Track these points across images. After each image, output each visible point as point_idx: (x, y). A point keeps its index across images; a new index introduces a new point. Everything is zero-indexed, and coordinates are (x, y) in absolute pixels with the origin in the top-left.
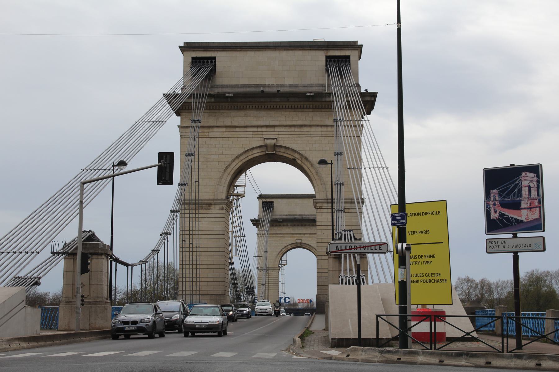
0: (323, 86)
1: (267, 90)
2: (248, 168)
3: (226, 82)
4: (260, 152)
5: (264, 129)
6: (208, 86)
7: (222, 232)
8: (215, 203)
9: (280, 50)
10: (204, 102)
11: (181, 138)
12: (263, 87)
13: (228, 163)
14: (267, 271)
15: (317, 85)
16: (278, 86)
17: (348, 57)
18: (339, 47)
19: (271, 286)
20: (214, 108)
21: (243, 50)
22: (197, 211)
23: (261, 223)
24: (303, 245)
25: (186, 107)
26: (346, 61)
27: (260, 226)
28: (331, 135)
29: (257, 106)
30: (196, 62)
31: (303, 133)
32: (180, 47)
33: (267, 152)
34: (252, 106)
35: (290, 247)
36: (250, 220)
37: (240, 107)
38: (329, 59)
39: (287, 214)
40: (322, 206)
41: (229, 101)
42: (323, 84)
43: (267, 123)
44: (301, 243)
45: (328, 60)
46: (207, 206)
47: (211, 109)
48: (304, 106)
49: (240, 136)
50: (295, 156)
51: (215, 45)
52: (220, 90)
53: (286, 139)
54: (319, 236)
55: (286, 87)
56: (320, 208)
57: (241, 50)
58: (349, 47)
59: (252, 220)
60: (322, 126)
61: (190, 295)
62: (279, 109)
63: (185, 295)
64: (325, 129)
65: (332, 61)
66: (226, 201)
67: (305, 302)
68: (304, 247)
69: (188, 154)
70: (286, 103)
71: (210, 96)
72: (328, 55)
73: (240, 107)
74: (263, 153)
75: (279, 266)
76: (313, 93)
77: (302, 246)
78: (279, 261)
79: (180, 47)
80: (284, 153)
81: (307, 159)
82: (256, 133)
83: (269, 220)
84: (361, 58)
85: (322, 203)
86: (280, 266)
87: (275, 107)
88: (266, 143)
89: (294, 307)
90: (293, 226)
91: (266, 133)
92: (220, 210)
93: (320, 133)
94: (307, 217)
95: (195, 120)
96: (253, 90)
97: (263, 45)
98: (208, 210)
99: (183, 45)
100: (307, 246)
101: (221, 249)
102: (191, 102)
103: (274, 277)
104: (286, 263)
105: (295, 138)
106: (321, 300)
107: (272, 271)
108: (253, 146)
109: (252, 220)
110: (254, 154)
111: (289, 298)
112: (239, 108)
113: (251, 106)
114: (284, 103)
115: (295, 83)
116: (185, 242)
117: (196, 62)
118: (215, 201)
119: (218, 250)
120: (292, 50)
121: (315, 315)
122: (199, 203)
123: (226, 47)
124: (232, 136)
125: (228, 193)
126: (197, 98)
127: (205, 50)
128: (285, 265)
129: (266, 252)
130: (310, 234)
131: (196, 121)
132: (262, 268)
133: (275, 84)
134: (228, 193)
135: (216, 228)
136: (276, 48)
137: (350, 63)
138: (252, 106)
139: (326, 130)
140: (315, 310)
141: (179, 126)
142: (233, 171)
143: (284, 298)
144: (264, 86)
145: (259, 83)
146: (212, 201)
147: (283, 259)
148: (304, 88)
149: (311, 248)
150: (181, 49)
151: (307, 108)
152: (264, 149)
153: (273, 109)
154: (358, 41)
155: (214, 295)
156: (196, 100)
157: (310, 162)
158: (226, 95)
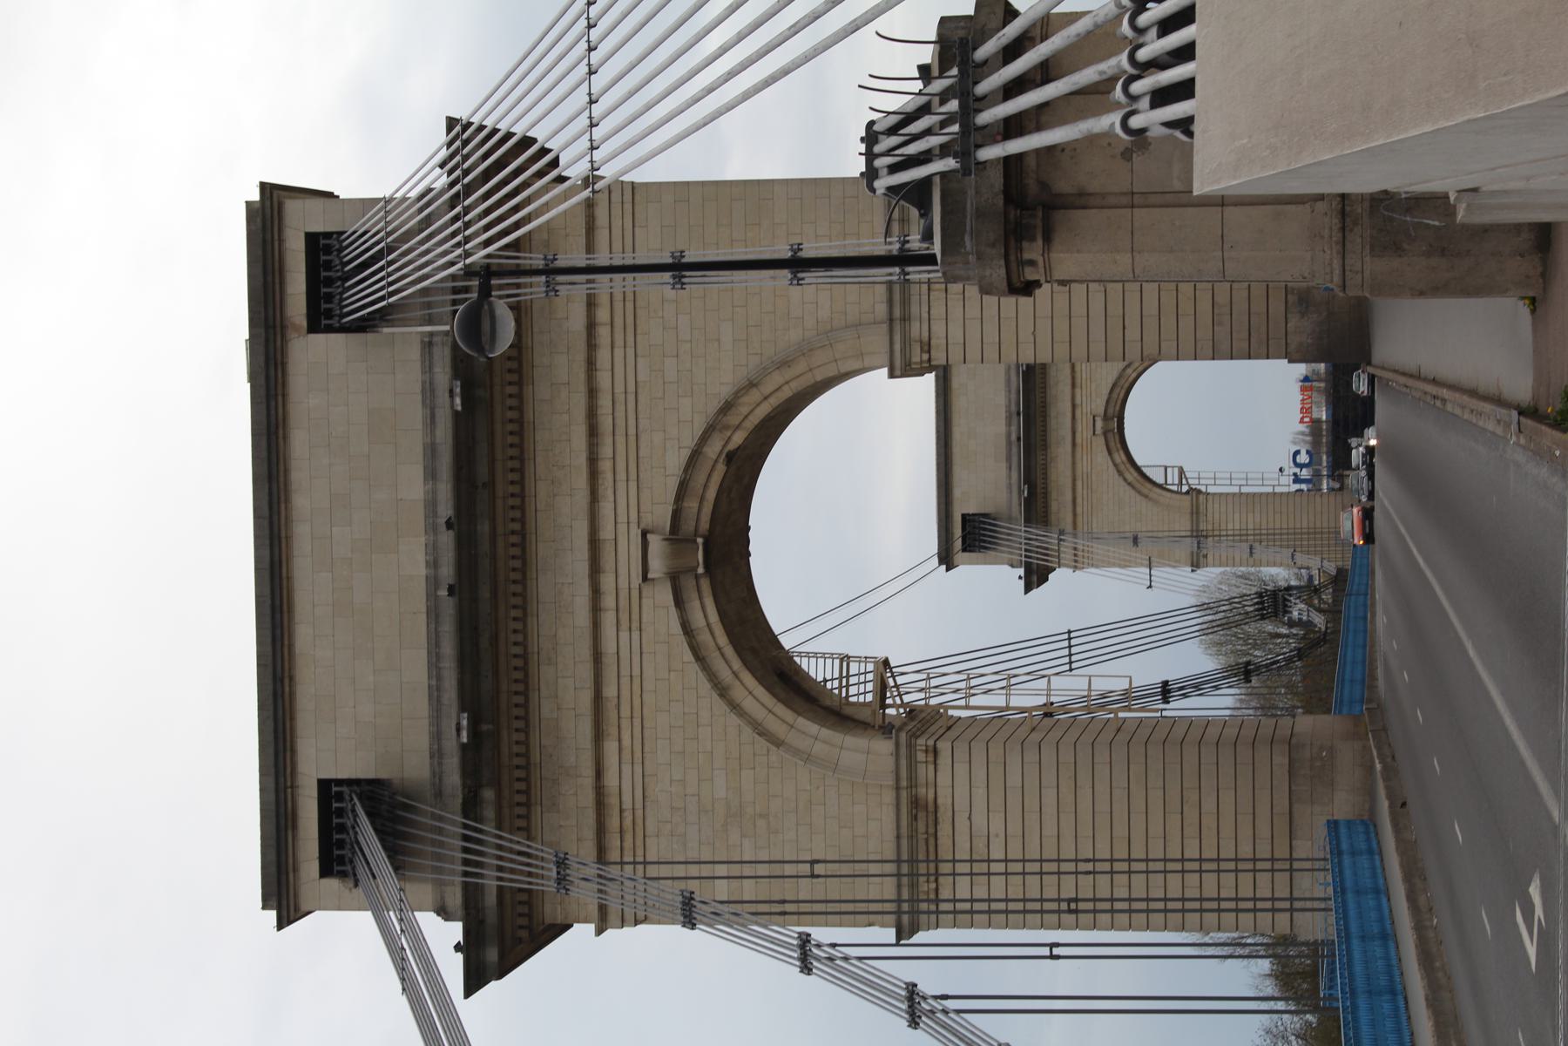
0: (428, 344)
1: (447, 572)
2: (774, 640)
3: (419, 740)
4: (701, 598)
5: (607, 582)
6: (434, 816)
7: (1031, 756)
8: (913, 783)
9: (286, 518)
11: (645, 920)
12: (436, 590)
13: (748, 731)
14: (1204, 533)
15: (428, 366)
16: (432, 528)
17: (312, 239)
18: (270, 279)
19: (1258, 520)
20: (522, 786)
21: (290, 669)
23: (1038, 559)
24: (1111, 411)
25: (520, 903)
26: (328, 250)
27: (1047, 561)
28: (630, 305)
29: (514, 613)
31: (621, 423)
32: (280, 926)
33: (701, 570)
34: (515, 631)
35: (1120, 457)
36: (1026, 593)
37: (516, 681)
38: (321, 318)
39: (1004, 465)
40: (921, 342)
41: (490, 727)
42: (422, 342)
44: (1106, 418)
45: (324, 322)
46: (921, 815)
47: (529, 799)
48: (511, 421)
49: (637, 681)
50: (715, 458)
51: (272, 786)
52: (453, 764)
53: (645, 494)
54: (1079, 351)
55: (434, 492)
56: (926, 348)
57: (291, 678)
58: (269, 236)
59: (1028, 588)
60: (591, 346)
61: (1292, 910)
62: (523, 521)
63: (1292, 899)
64: (603, 333)
65: (328, 306)
66: (903, 736)
67: (1309, 401)
68: (1117, 408)
69: (685, 917)
70: (500, 493)
71: (471, 807)
72: (305, 324)
73: (516, 681)
74: (705, 585)
75: (1187, 493)
76: (454, 382)
77: (1116, 414)
78: (1169, 494)
79: (280, 926)
81: (727, 407)
83: (1025, 531)
84: (333, 193)
85: (906, 342)
86: (1185, 488)
87: (514, 539)
88: (662, 575)
89: (1324, 433)
91: (623, 571)
92: (938, 762)
93: (619, 353)
94: (1013, 396)
95: (554, 874)
96: (448, 628)
97: (267, 591)
98: (941, 810)
99: (272, 915)
100: (1115, 395)
101: (1102, 756)
102: (500, 888)
103: (1223, 509)
104: (1176, 470)
105: (641, 454)
106: (1309, 341)
107: (1202, 518)
108: (676, 628)
109: (1028, 589)
110: (708, 625)
111: (1297, 453)
112: (520, 687)
113: (513, 638)
114: (499, 503)
115: (421, 458)
116: (1064, 912)
117: (341, 860)
118: (904, 783)
119: (1102, 771)
120: (286, 471)
121: (1376, 367)
122: (913, 861)
123: (276, 738)
124: (637, 714)
125: (874, 727)
127: (290, 824)
128: (1181, 472)
129: (1135, 540)
130: (1073, 386)
131: (558, 873)
132: (1192, 553)
133: (423, 539)
135: (1014, 779)
136: (280, 538)
138: (515, 631)
139: (609, 327)
140: (1335, 367)
141: (599, 932)
142: (780, 709)
143: (1297, 470)
144: (433, 582)
146: (904, 794)
147: (1160, 480)
148: (437, 420)
149: (1122, 381)
150: (290, 922)
151: (520, 409)
152: (688, 583)
153: (523, 545)
154: (246, 202)
155: (1293, 788)
156: (492, 870)
157: (739, 393)
158: (465, 740)
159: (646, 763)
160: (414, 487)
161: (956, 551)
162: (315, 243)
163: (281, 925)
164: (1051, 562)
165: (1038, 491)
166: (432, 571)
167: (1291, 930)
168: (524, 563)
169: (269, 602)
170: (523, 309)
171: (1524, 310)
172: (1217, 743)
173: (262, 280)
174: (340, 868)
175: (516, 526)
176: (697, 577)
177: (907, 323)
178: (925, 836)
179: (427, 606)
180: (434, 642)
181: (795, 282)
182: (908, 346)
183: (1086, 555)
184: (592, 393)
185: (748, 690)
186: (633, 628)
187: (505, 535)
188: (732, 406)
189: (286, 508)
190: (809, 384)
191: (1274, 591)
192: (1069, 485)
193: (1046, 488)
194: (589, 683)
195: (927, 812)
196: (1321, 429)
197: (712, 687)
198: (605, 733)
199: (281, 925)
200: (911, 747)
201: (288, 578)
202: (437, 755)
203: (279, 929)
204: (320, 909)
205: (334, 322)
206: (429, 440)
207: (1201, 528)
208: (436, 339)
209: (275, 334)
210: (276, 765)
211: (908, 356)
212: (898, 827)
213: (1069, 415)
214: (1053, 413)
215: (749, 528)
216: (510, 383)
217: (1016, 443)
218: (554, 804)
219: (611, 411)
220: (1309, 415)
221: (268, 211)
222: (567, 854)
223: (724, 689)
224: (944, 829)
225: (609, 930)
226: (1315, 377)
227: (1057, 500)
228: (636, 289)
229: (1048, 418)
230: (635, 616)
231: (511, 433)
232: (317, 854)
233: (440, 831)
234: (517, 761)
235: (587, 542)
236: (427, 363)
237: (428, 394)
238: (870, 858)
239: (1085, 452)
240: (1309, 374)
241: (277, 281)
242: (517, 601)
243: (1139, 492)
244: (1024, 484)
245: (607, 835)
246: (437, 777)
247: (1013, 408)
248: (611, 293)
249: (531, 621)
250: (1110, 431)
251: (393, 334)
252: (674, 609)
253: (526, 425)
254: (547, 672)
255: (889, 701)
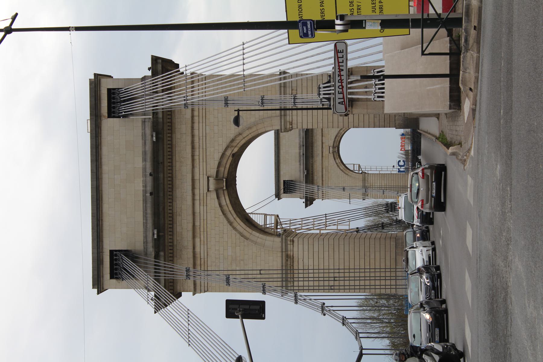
0: (144, 122)
1: (149, 189)
2: (244, 210)
3: (140, 238)
4: (224, 196)
5: (197, 192)
6: (145, 259)
8: (286, 250)
10: (165, 264)
11: (207, 291)
13: (238, 235)
16: (144, 176)
17: (109, 90)
18: (97, 102)
19: (385, 183)
22: (296, 272)
23: (310, 195)
24: (335, 145)
26: (114, 93)
27: (313, 196)
29: (169, 201)
30: (116, 274)
31: (201, 145)
32: (98, 294)
33: (225, 188)
34: (170, 206)
35: (338, 161)
38: (111, 114)
39: (298, 163)
41: (163, 234)
42: (142, 121)
43: (190, 188)
44: (333, 147)
46: (289, 260)
47: (173, 255)
49: (205, 221)
50: (229, 155)
53: (208, 166)
54: (325, 125)
55: (145, 165)
56: (291, 124)
57: (102, 220)
58: (96, 89)
60: (193, 123)
64: (196, 119)
66: (284, 236)
67: (404, 142)
68: (337, 144)
69: (227, 282)
71: (157, 256)
72: (107, 115)
74: (226, 192)
75: (361, 173)
76: (153, 133)
77: (337, 146)
79: (98, 294)
80: (225, 167)
81: (233, 141)
82: (202, 202)
83: (306, 186)
84: (111, 76)
86: (360, 172)
87: (169, 179)
88: (213, 190)
90: (312, 157)
91: (201, 188)
93: (201, 124)
94: (301, 140)
95: (186, 274)
96: (149, 205)
99: (96, 290)
100: (336, 140)
101: (342, 242)
103: (374, 179)
105: (207, 154)
107: (366, 182)
109: (306, 206)
110: (227, 204)
111: (399, 161)
113: (169, 208)
114: (165, 168)
116: (333, 286)
117: (116, 274)
118: (284, 250)
119: (342, 246)
120: (101, 159)
121: (420, 130)
124: (205, 230)
126: (159, 273)
127: (101, 263)
128: (359, 166)
129: (344, 189)
130: (322, 136)
131: (187, 274)
133: (142, 179)
134: (274, 235)
135: (316, 249)
136: (99, 178)
137: (116, 89)
138: (170, 206)
139: (198, 117)
141: (194, 294)
142: (248, 229)
143: (400, 168)
144: (145, 192)
145: (141, 198)
146: (284, 253)
147: (352, 169)
148: (146, 144)
149: (339, 135)
150: (101, 292)
151: (171, 141)
152: (221, 192)
153: (172, 181)
154: (90, 79)
157: (236, 137)
158: (156, 237)
159: (208, 245)
160: (139, 163)
161: (281, 194)
162: (110, 92)
163: (99, 293)
164: (314, 196)
165: (310, 172)
166: (145, 188)
167: (396, 292)
168: (172, 186)
169: (95, 197)
170: (173, 112)
171: (436, 119)
172: (375, 238)
173: (94, 102)
174: (116, 276)
175: (170, 175)
176: (223, 190)
177: (286, 116)
178: (290, 266)
179: (143, 199)
180: (145, 209)
181: (262, 106)
182: (286, 123)
183: (326, 195)
184: (193, 136)
185: (238, 223)
186: (204, 205)
187: (167, 178)
188: (234, 140)
189: (101, 169)
190: (257, 134)
191: (391, 203)
192: (321, 170)
193: (312, 171)
194: (191, 221)
195: (290, 259)
196: (408, 153)
197: (228, 222)
198: (196, 236)
199: (99, 293)
200: (286, 240)
201: (101, 190)
202: (145, 243)
203: (98, 294)
204: (110, 289)
205: (116, 115)
206: (144, 150)
207: (366, 185)
208: (147, 120)
209: (98, 118)
210: (97, 246)
211: (286, 126)
212: (282, 263)
213: (321, 146)
214: (315, 145)
215: (236, 177)
216: (169, 133)
217: (302, 156)
218: (181, 257)
219: (198, 142)
220: (404, 148)
221: (96, 82)
222: (189, 268)
223: (231, 223)
224: (296, 264)
225: (197, 294)
226: (407, 134)
227: (316, 176)
228: (206, 107)
229: (313, 147)
230: (205, 202)
231: (169, 148)
232: (109, 272)
233: (147, 264)
234: (170, 244)
235: (191, 180)
236: (144, 127)
237: (144, 136)
238: (278, 269)
239: (326, 159)
240: (404, 133)
241: (99, 102)
242: (170, 197)
243: (345, 173)
244: (305, 170)
245: (196, 266)
246: (146, 249)
247: (301, 144)
248: (199, 108)
249: (174, 203)
250: (335, 152)
251: (133, 118)
252: (217, 199)
253: (173, 145)
254: (178, 219)
255: (279, 227)
